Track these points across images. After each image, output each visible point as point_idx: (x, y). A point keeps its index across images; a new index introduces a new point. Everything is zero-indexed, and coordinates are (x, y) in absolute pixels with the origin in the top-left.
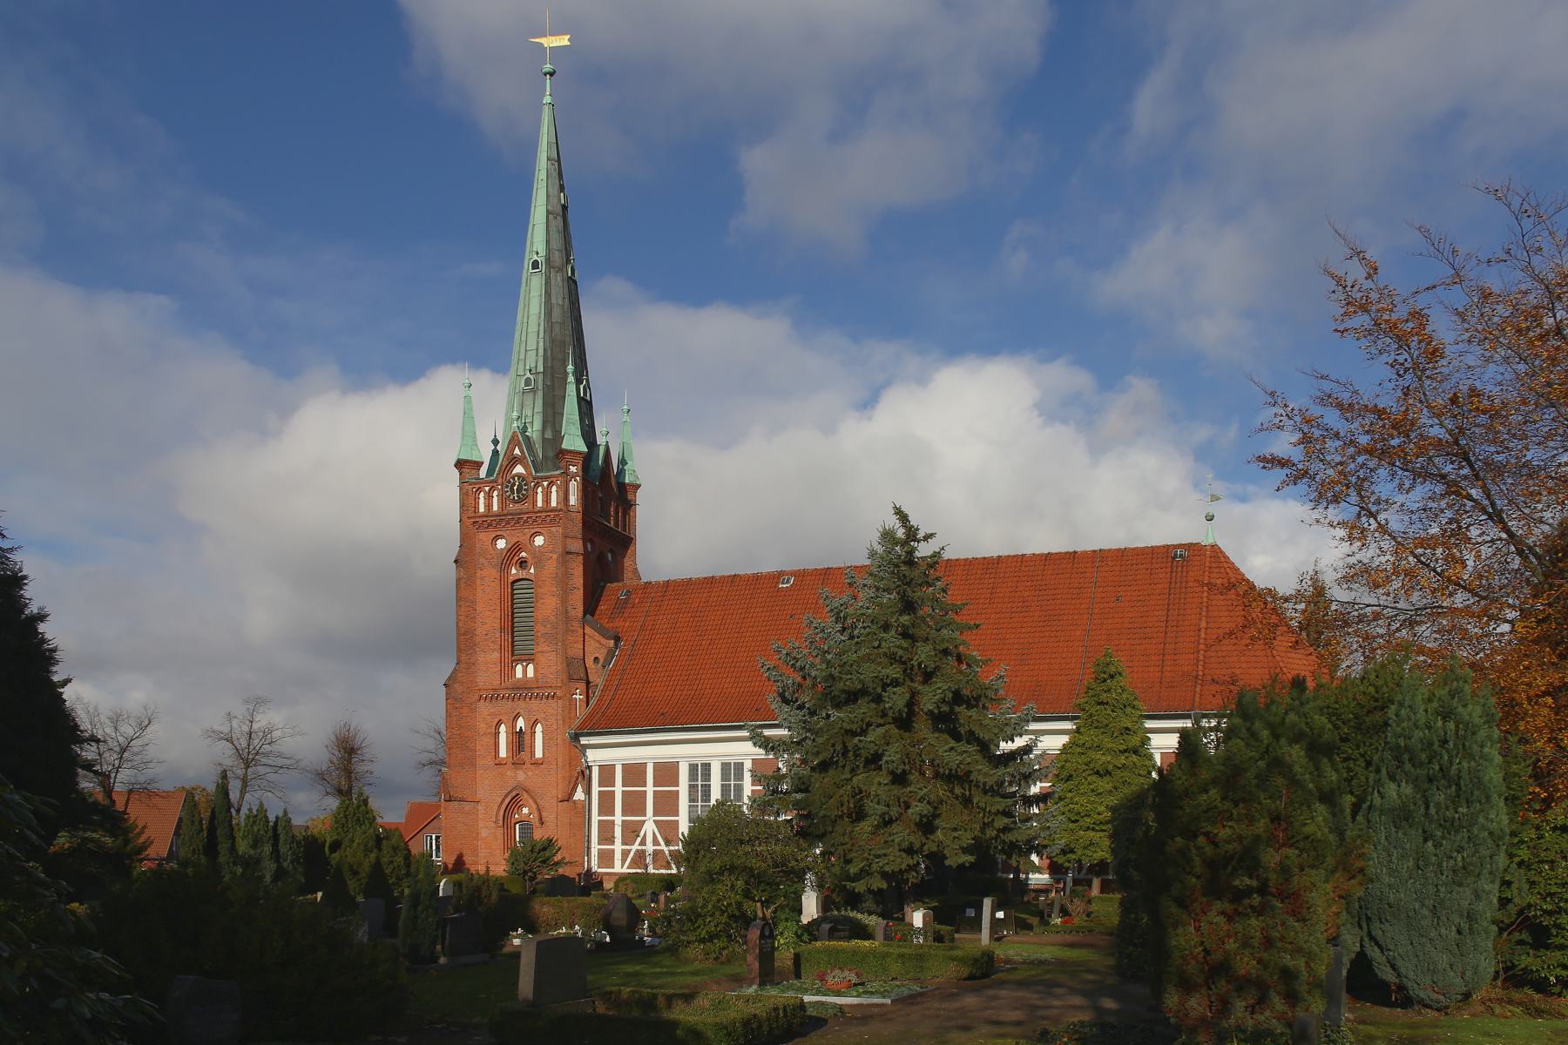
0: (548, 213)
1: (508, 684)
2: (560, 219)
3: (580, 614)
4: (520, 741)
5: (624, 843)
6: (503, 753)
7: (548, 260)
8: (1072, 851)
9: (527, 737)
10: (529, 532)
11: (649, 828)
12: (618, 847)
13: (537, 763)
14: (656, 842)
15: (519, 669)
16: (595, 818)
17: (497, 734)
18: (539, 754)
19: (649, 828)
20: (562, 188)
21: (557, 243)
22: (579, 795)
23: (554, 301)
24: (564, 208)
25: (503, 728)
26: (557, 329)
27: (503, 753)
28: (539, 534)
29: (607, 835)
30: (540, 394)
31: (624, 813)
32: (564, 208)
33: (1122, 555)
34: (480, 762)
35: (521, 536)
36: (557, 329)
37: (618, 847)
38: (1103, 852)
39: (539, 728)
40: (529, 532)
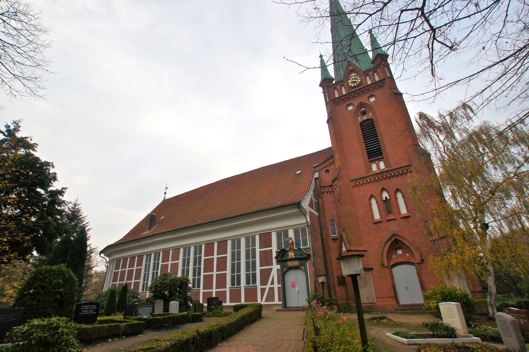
4: (388, 206)
5: (273, 288)
6: (377, 216)
13: (406, 217)
15: (374, 167)
18: (404, 211)
25: (373, 201)
27: (377, 216)
28: (371, 96)
35: (363, 99)
39: (399, 196)
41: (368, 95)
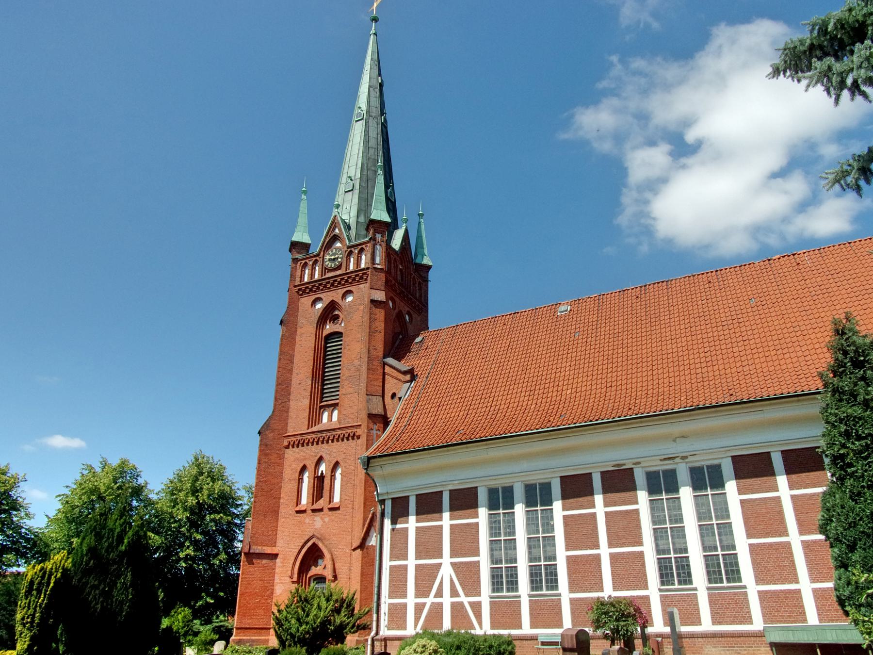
0: (370, 87)
1: (315, 429)
2: (378, 90)
3: (381, 355)
7: (368, 111)
8: (335, 238)
9: (327, 481)
10: (341, 291)
11: (446, 572)
12: (411, 600)
14: (454, 593)
15: (325, 416)
16: (387, 563)
17: (300, 480)
19: (446, 572)
20: (380, 75)
21: (375, 102)
22: (373, 541)
23: (371, 134)
24: (381, 85)
25: (306, 476)
26: (371, 151)
29: (399, 589)
30: (357, 192)
31: (418, 557)
32: (381, 85)
33: (513, 497)
34: (283, 511)
35: (335, 295)
36: (371, 151)
37: (411, 600)
38: (811, 434)
39: (339, 472)
40: (341, 291)
41: (314, 297)
